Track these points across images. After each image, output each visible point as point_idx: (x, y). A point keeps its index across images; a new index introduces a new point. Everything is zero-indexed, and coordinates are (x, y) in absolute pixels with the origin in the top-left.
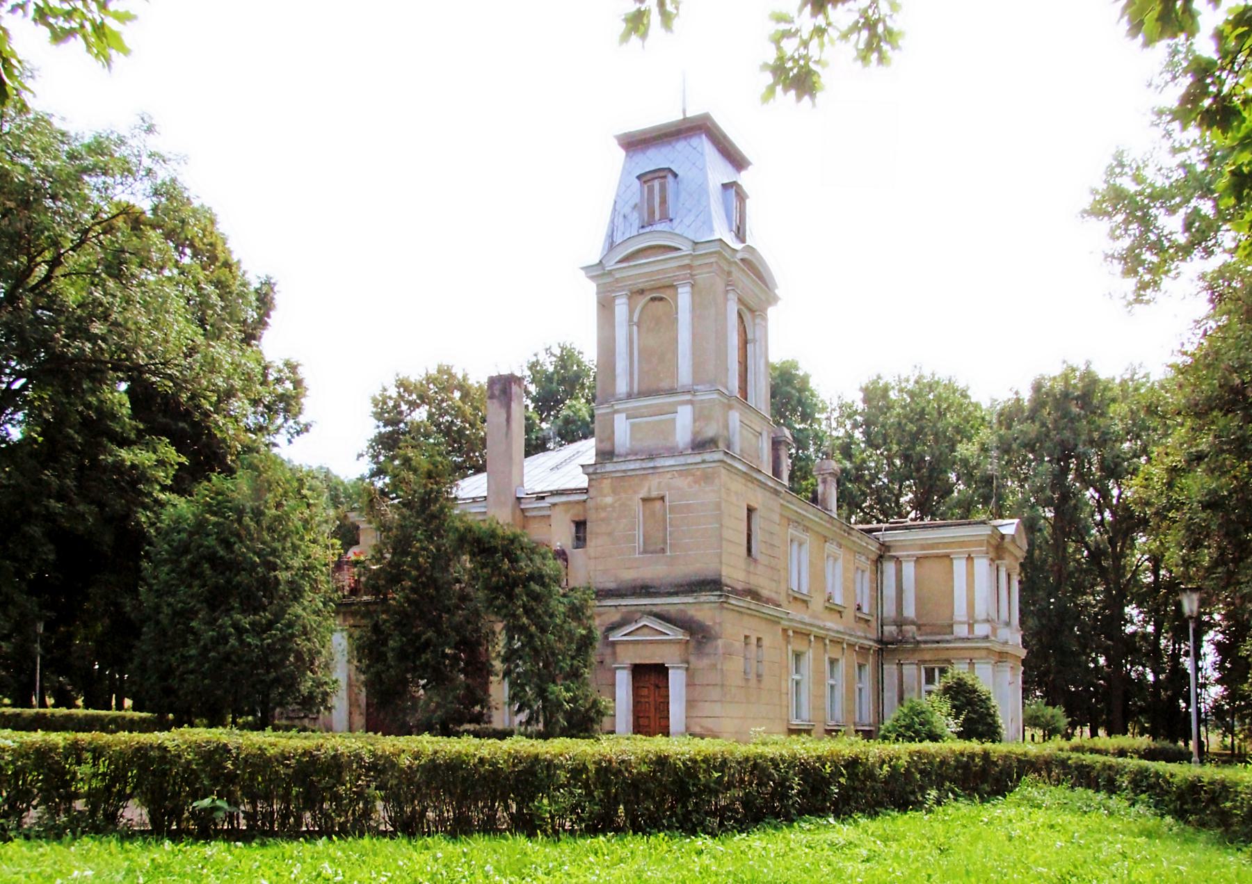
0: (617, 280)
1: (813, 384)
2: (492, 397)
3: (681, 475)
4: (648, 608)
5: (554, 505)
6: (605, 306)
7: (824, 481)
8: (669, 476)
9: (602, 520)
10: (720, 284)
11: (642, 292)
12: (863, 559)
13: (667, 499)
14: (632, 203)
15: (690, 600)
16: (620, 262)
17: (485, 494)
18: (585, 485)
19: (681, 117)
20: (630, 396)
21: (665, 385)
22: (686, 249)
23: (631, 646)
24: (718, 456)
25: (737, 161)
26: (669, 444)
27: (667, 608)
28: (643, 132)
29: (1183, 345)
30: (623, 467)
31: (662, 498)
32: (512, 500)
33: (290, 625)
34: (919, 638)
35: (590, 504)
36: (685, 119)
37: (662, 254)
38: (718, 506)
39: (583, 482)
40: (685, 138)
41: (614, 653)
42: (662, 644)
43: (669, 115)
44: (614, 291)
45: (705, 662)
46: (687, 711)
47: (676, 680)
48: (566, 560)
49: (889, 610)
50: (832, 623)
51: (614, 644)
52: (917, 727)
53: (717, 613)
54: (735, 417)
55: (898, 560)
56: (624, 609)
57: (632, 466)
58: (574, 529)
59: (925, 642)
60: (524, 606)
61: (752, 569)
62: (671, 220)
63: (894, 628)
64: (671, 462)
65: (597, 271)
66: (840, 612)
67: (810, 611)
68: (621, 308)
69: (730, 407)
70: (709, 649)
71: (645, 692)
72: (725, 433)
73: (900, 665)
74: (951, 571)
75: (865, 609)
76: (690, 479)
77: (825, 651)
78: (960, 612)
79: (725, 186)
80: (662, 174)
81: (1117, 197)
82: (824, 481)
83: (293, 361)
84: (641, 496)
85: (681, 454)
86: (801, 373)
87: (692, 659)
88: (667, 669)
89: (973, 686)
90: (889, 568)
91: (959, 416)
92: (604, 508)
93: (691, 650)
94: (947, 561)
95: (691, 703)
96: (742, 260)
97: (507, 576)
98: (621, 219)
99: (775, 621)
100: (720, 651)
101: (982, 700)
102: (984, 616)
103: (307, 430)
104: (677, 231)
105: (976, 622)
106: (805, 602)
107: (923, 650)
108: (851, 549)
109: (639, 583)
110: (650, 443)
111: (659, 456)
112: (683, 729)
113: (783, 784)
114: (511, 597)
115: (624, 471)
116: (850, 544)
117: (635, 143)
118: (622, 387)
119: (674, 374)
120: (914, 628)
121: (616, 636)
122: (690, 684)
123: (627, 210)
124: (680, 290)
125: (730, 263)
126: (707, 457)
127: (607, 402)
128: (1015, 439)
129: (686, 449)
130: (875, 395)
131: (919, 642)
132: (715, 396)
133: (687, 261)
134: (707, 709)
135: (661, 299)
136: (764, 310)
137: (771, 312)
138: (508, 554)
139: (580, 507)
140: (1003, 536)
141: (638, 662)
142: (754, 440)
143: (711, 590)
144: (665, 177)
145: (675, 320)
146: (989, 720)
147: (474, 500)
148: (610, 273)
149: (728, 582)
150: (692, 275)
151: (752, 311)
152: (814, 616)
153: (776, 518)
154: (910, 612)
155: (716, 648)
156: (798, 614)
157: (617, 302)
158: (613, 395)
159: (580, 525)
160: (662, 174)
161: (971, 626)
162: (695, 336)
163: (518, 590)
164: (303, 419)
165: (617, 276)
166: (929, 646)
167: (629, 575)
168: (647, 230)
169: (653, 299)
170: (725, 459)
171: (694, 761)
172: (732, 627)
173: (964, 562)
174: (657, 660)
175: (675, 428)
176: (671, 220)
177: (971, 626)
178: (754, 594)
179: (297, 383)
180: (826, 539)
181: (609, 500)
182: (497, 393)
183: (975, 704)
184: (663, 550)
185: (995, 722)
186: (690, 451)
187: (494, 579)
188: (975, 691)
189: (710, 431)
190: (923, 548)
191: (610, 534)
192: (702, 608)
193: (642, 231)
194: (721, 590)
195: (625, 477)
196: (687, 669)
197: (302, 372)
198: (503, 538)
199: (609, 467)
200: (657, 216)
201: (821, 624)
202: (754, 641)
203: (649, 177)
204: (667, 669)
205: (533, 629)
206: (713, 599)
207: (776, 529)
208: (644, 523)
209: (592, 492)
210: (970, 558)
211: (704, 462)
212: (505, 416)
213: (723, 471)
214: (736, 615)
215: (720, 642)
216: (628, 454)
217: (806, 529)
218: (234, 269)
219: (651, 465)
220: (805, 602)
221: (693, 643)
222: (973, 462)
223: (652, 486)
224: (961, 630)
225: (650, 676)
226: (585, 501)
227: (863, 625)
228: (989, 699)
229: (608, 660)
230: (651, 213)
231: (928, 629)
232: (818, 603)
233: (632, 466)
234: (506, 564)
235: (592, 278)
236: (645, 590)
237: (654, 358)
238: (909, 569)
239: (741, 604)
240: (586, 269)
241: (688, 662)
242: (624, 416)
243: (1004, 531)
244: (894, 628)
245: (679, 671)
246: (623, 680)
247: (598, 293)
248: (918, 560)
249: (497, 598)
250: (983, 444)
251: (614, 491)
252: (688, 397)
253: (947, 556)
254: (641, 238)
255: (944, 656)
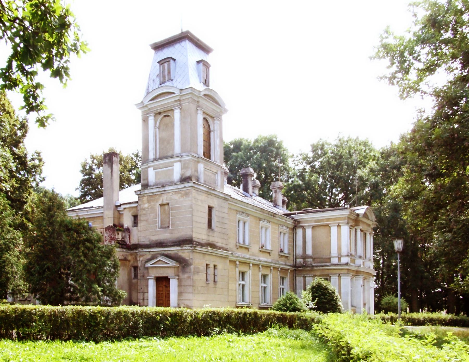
0: (149, 109)
1: (284, 145)
2: (105, 163)
3: (176, 194)
4: (163, 252)
5: (125, 208)
6: (145, 120)
7: (276, 192)
8: (171, 194)
9: (144, 214)
10: (193, 107)
11: (160, 113)
12: (284, 228)
13: (170, 204)
14: (157, 74)
15: (179, 248)
16: (150, 100)
17: (103, 205)
18: (137, 200)
19: (180, 32)
20: (155, 160)
21: (170, 154)
22: (177, 92)
23: (155, 269)
24: (191, 184)
25: (204, 49)
26: (171, 180)
27: (170, 252)
28: (161, 42)
29: (33, 156)
30: (152, 191)
31: (168, 204)
32: (113, 207)
33: (4, 262)
34: (313, 265)
35: (139, 208)
36: (182, 33)
37: (167, 96)
38: (191, 207)
39: (136, 198)
40: (179, 42)
41: (148, 272)
42: (167, 268)
43: (175, 32)
44: (148, 114)
45: (186, 276)
46: (178, 297)
47: (173, 284)
48: (130, 232)
49: (299, 251)
50: (264, 258)
51: (147, 268)
52: (288, 305)
53: (191, 254)
54: (201, 167)
55: (303, 228)
56: (152, 253)
57: (155, 190)
58: (133, 219)
59: (316, 266)
60: (83, 252)
61: (210, 234)
62: (172, 80)
63: (301, 260)
64: (171, 188)
65: (142, 106)
66: (269, 253)
67: (250, 253)
68: (151, 120)
69: (198, 162)
70: (188, 270)
71: (161, 289)
72: (196, 174)
73: (304, 277)
74: (330, 232)
75: (286, 251)
76: (180, 195)
77: (259, 271)
78: (334, 251)
79: (198, 62)
80: (168, 60)
81: (387, 49)
82: (276, 192)
83: (39, 151)
84: (159, 203)
85: (176, 184)
86: (278, 140)
87: (180, 274)
88: (169, 279)
89: (325, 286)
90: (300, 232)
91: (360, 155)
92: (144, 209)
93: (180, 270)
94: (328, 227)
95: (180, 294)
96: (205, 95)
97: (76, 240)
98: (152, 81)
99: (225, 258)
100: (192, 270)
101: (330, 293)
102: (346, 254)
103: (44, 180)
104: (175, 85)
105: (342, 256)
106: (247, 249)
107: (316, 270)
108: (276, 223)
109: (159, 241)
110: (163, 180)
111: (166, 185)
112: (176, 305)
113: (136, 323)
114: (78, 249)
115: (153, 193)
116: (276, 221)
117: (158, 47)
118: (151, 156)
119: (173, 150)
120: (311, 260)
121: (149, 265)
122: (180, 286)
123: (155, 77)
124: (175, 111)
125: (198, 97)
126: (186, 185)
127: (145, 163)
128: (389, 165)
129: (178, 182)
130: (318, 149)
131: (313, 266)
132: (190, 158)
133: (178, 98)
134: (186, 296)
135: (168, 116)
136: (221, 116)
137: (224, 117)
138: (78, 232)
139: (135, 209)
140: (358, 215)
141: (157, 276)
142: (213, 176)
143: (188, 244)
144: (169, 61)
145: (173, 126)
146: (333, 302)
147: (99, 208)
148: (146, 106)
149: (196, 240)
150: (180, 104)
151: (212, 117)
152: (253, 255)
153: (226, 210)
154: (309, 252)
155: (190, 269)
156: (240, 254)
157: (150, 118)
158: (148, 160)
159: (135, 217)
160: (168, 60)
161: (339, 259)
162: (182, 132)
163: (81, 246)
164: (43, 175)
165: (149, 107)
166: (318, 268)
167: (155, 238)
168: (162, 85)
169: (165, 116)
170: (194, 185)
171: (95, 313)
172: (198, 260)
173: (336, 228)
174: (165, 275)
175: (173, 174)
176: (172, 80)
177: (339, 259)
178: (212, 246)
179: (40, 160)
180: (260, 219)
181: (146, 206)
182: (107, 161)
183: (326, 295)
184: (169, 227)
185: (336, 303)
186: (179, 183)
187: (71, 241)
188: (327, 289)
189: (188, 174)
190: (316, 221)
191: (147, 220)
192: (184, 252)
193: (160, 86)
194: (192, 244)
195: (153, 195)
196: (178, 279)
197: (42, 156)
198: (75, 224)
199: (146, 191)
200: (167, 79)
201: (257, 258)
202: (212, 266)
203: (163, 62)
204: (169, 279)
205: (86, 261)
206: (188, 248)
207: (226, 216)
208: (161, 215)
209: (140, 203)
210: (339, 226)
211: (185, 187)
212: (110, 171)
213: (194, 191)
214: (202, 255)
215: (192, 267)
216: (153, 186)
217: (248, 215)
218: (12, 114)
219: (163, 189)
220: (247, 249)
221: (180, 268)
222: (366, 178)
223: (164, 199)
224: (334, 261)
225: (163, 282)
226: (137, 207)
227: (284, 259)
228: (334, 293)
229: (146, 275)
230: (164, 77)
231: (318, 260)
232: (255, 249)
233: (155, 190)
234: (75, 235)
235: (139, 108)
236: (160, 244)
237: (165, 142)
238: (309, 232)
239: (206, 250)
240: (137, 105)
241: (178, 276)
242: (152, 168)
243: (358, 212)
244: (301, 260)
245: (174, 280)
246: (152, 284)
247: (142, 115)
248: (313, 227)
249: (72, 249)
250: (372, 169)
251: (149, 202)
252: (179, 159)
253: (327, 225)
254: (161, 88)
255: (326, 273)
